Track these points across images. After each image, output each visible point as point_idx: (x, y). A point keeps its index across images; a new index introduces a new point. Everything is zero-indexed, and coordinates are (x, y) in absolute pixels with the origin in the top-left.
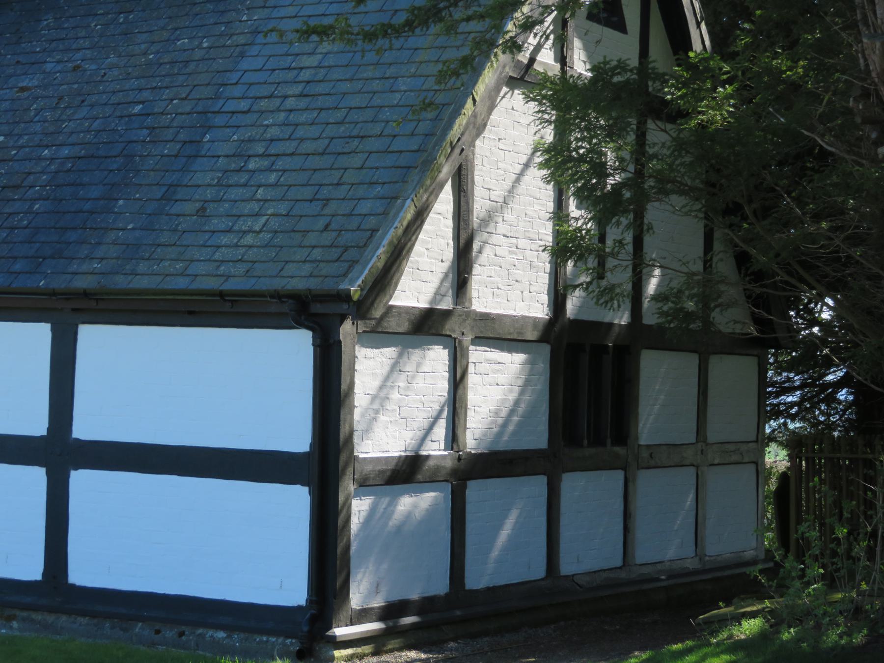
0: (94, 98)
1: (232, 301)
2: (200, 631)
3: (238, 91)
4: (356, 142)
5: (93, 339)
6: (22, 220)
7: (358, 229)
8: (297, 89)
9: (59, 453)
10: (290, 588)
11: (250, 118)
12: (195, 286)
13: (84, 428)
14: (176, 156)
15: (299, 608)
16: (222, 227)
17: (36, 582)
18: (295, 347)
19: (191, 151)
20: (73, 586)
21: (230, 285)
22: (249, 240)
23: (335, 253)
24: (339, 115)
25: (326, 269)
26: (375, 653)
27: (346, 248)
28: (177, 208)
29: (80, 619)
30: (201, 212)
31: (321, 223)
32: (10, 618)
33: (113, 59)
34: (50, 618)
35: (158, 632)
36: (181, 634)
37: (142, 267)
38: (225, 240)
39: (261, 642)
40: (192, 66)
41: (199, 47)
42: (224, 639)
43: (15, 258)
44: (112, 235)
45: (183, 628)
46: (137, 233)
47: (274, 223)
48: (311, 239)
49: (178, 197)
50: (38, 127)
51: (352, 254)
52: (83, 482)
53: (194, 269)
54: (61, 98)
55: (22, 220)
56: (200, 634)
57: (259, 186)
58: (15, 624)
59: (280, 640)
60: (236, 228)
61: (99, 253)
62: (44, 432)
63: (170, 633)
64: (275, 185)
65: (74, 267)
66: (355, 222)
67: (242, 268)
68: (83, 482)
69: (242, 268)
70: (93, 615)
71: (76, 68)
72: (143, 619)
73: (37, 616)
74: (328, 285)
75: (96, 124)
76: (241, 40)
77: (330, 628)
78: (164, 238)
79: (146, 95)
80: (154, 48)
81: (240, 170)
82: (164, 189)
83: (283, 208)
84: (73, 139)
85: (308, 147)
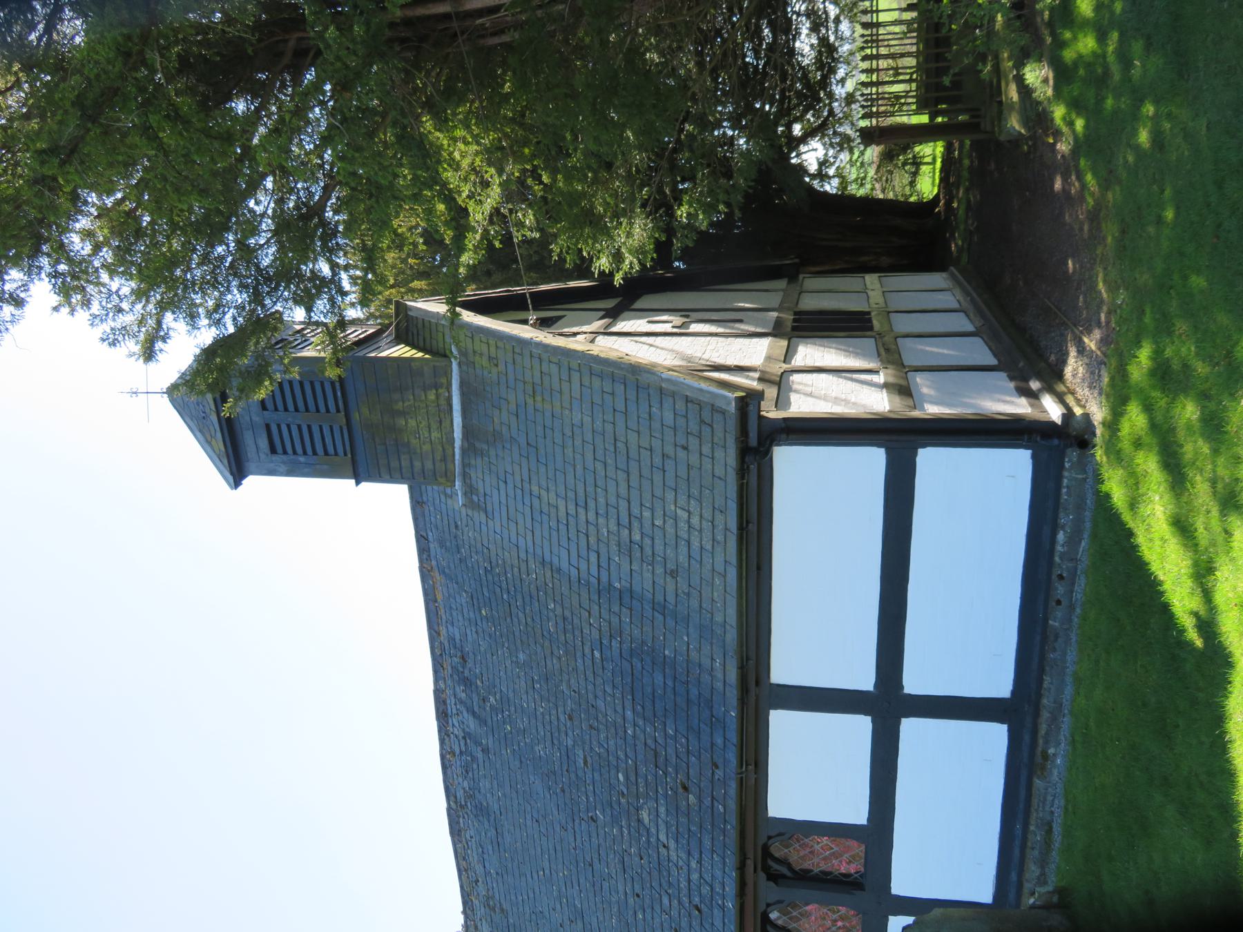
0: (591, 696)
1: (748, 522)
2: (1057, 559)
3: (583, 566)
4: (619, 444)
5: (786, 668)
6: (681, 745)
7: (686, 417)
8: (581, 511)
9: (887, 705)
10: (1015, 466)
11: (603, 550)
12: (733, 559)
13: (864, 679)
14: (631, 610)
15: (1034, 457)
16: (686, 549)
17: (1009, 730)
18: (791, 464)
19: (627, 596)
20: (1013, 692)
21: (733, 524)
22: (695, 521)
23: (706, 431)
24: (599, 466)
25: (719, 433)
26: (1073, 393)
27: (702, 421)
28: (671, 598)
29: (1046, 685)
30: (674, 574)
31: (682, 454)
32: (1045, 756)
33: (564, 687)
34: (1045, 715)
35: (1059, 602)
36: (1061, 577)
37: (719, 618)
38: (695, 544)
39: (1068, 493)
40: (567, 614)
41: (554, 611)
42: (1065, 532)
43: (712, 744)
44: (694, 655)
45: (1054, 577)
46: (691, 630)
47: (682, 500)
48: (694, 459)
49: (662, 599)
50: (612, 743)
51: (706, 415)
52: (915, 682)
53: (720, 567)
54: (591, 727)
55: (681, 745)
56: (1061, 558)
57: (653, 524)
58: (1051, 751)
59: (1066, 474)
60: (686, 536)
61: (706, 662)
62: (869, 719)
63: (1060, 590)
64: (652, 510)
65: (719, 685)
66: (681, 422)
67: (719, 518)
68: (915, 682)
69: (719, 518)
70: (1042, 671)
71: (571, 718)
72: (1046, 620)
73: (1043, 729)
74: (732, 425)
75: (609, 690)
76: (548, 574)
77: (1053, 423)
78: (695, 603)
79: (587, 651)
80: (556, 652)
81: (641, 548)
82: (656, 614)
83: (670, 496)
84: (619, 709)
85: (623, 491)
